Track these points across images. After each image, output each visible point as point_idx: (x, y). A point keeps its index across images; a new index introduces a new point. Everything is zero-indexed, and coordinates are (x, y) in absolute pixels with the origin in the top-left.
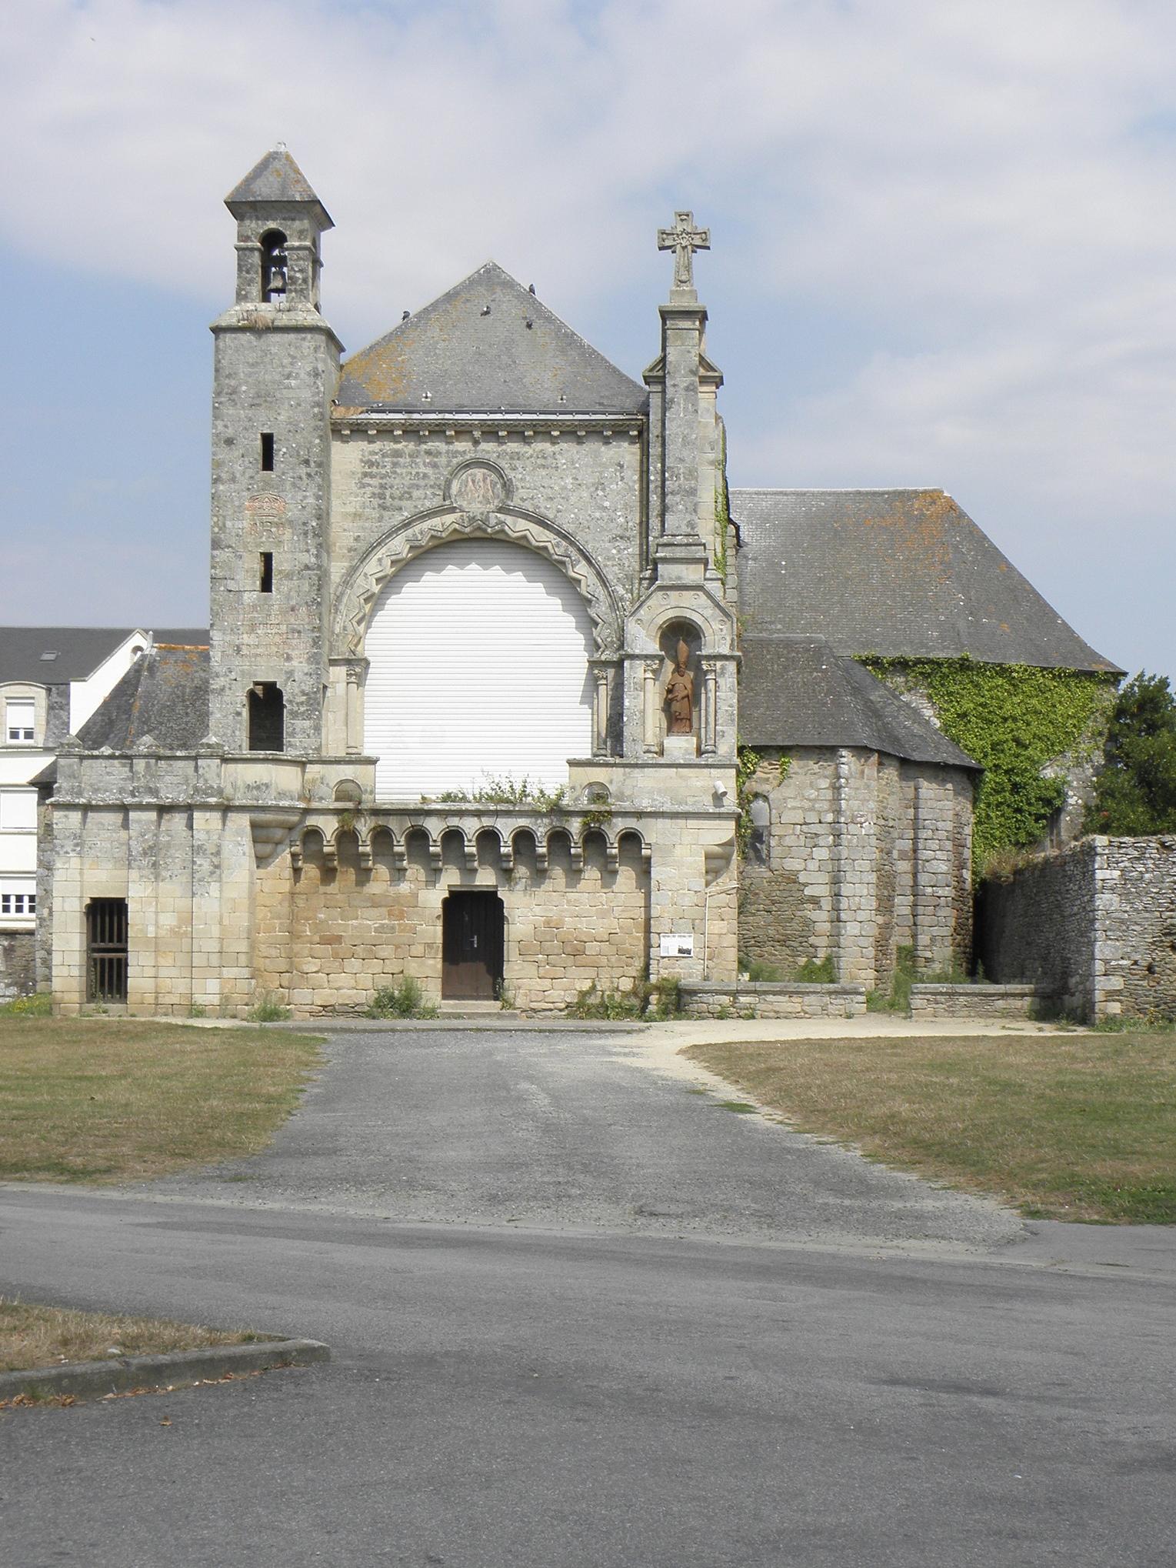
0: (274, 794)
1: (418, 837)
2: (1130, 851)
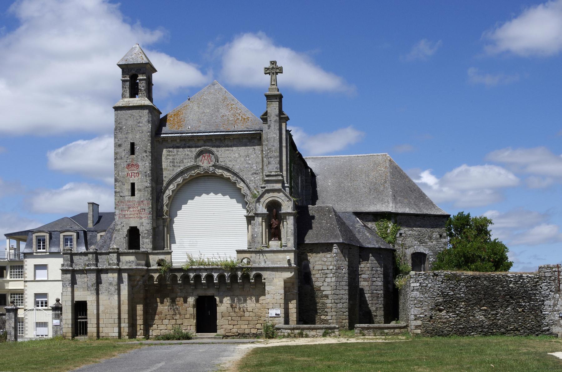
2: (423, 276)
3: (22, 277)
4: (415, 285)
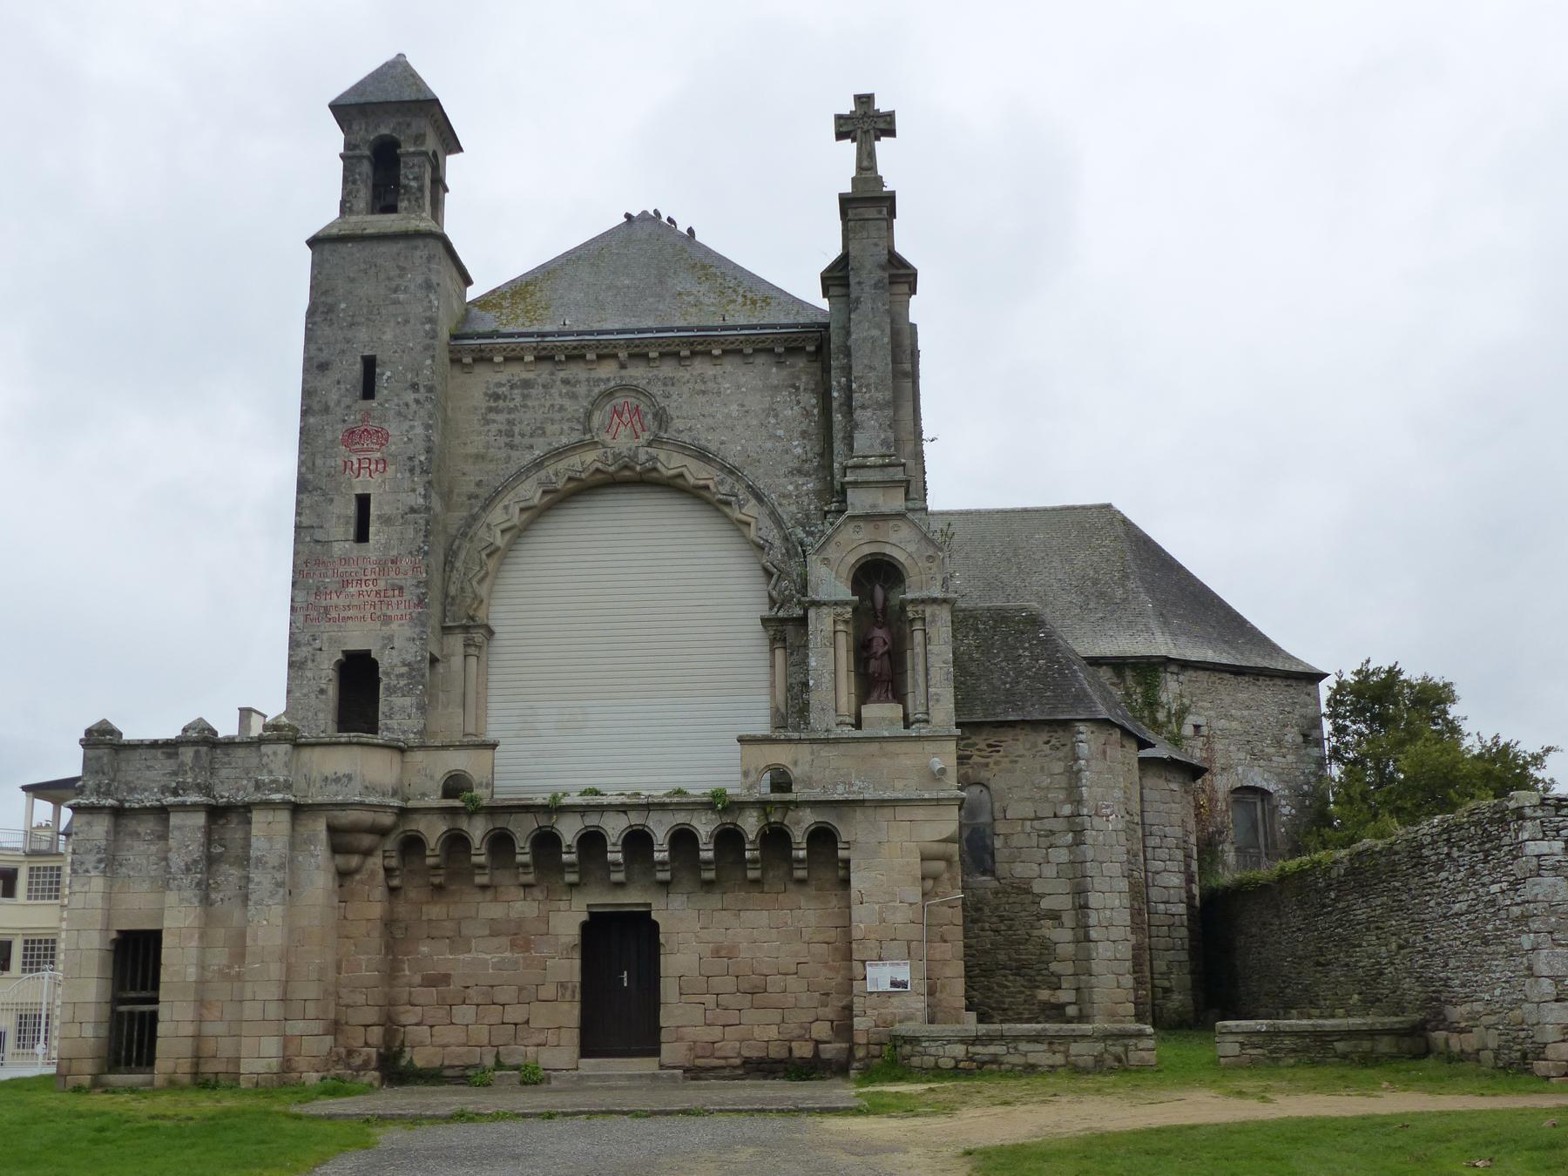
0: (359, 788)
1: (546, 841)
3: (57, 897)
4: (1544, 847)
